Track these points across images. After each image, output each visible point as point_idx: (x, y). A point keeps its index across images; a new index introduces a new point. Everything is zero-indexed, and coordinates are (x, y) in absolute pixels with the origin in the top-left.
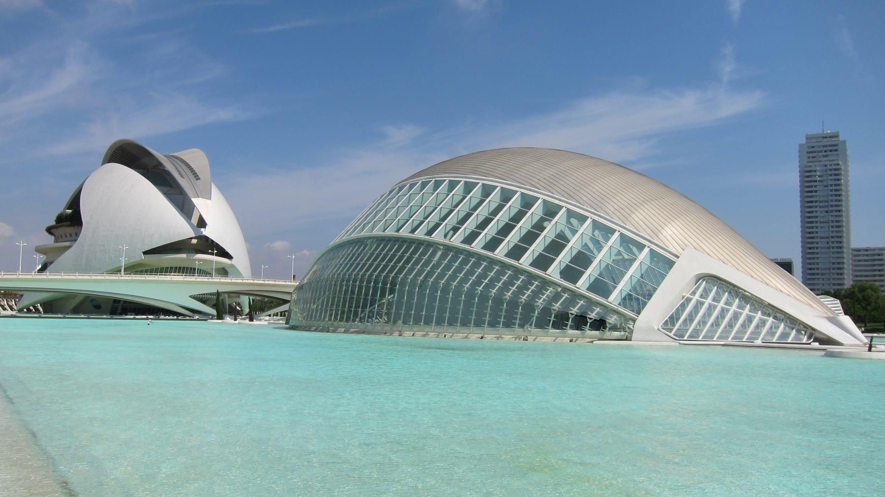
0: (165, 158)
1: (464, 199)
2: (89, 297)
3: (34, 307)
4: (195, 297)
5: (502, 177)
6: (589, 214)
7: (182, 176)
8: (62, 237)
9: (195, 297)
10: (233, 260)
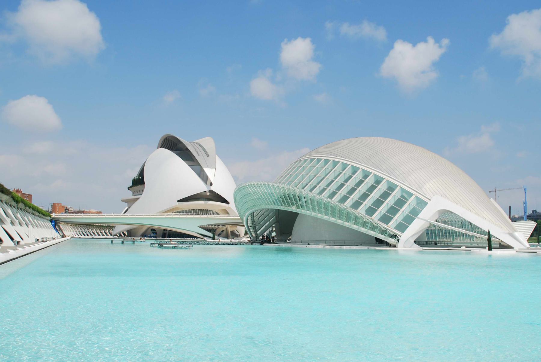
0: (189, 143)
1: (341, 174)
2: (149, 227)
3: (123, 233)
4: (201, 227)
5: (344, 156)
6: (399, 183)
7: (198, 155)
8: (135, 193)
9: (201, 227)
10: (230, 204)
